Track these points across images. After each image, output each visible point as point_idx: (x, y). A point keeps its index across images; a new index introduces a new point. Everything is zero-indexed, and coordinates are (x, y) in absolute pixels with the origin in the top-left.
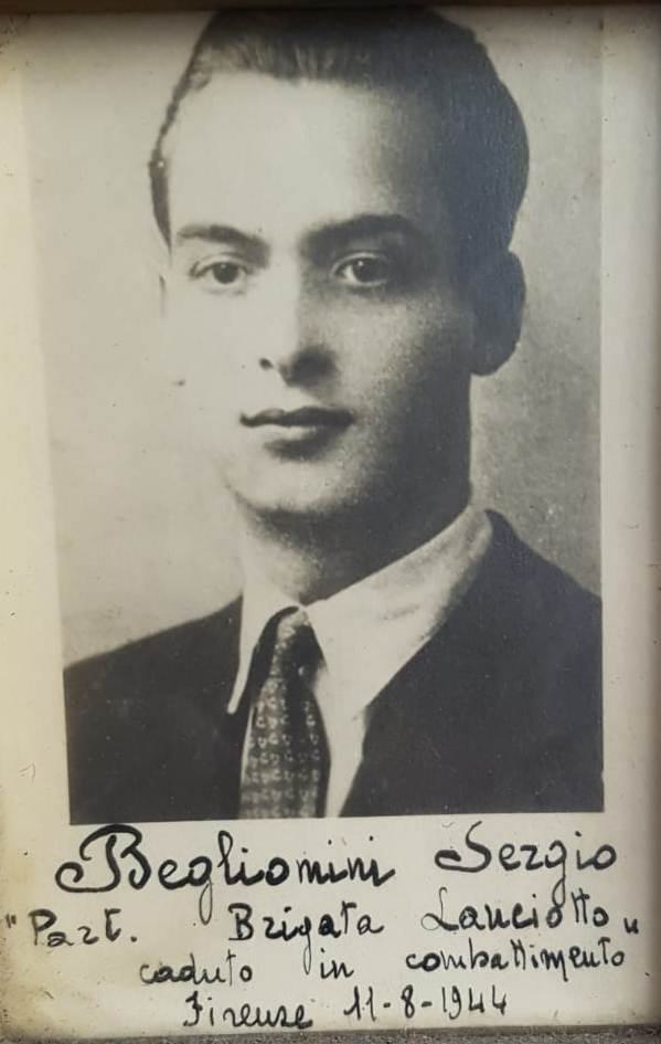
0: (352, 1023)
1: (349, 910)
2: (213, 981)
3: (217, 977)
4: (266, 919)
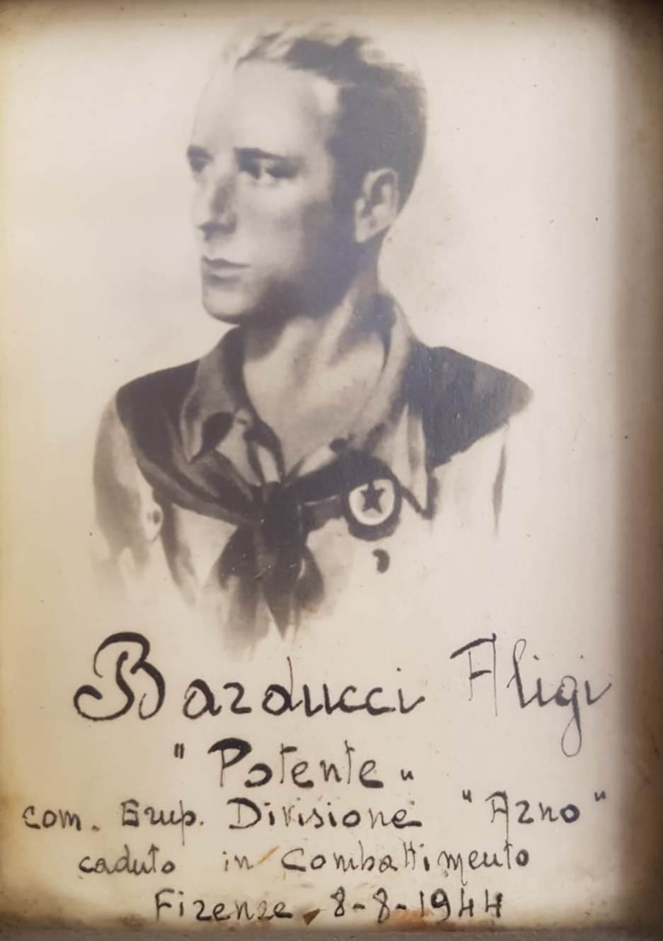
2: (168, 823)
4: (494, 636)
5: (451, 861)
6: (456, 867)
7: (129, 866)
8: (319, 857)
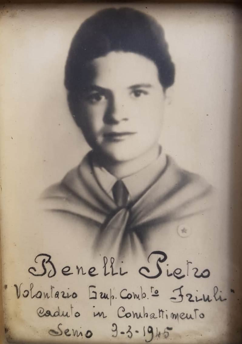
2: (65, 316)
3: (67, 315)
4: (129, 326)
5: (174, 316)
6: (176, 318)
8: (183, 313)
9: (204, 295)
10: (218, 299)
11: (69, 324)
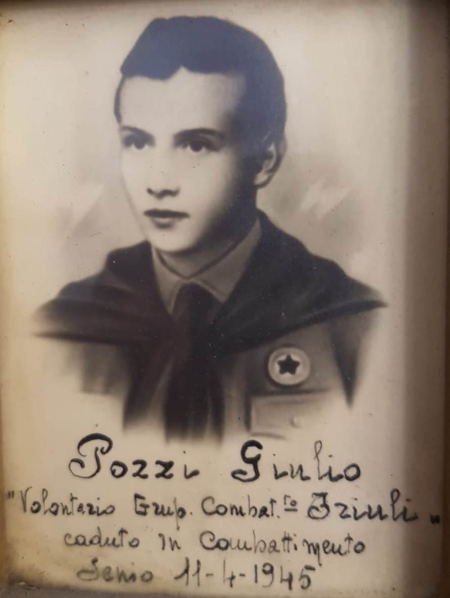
0: (179, 586)
1: (287, 498)
5: (311, 548)
7: (221, 546)
9: (291, 466)
10: (325, 475)
11: (113, 559)
